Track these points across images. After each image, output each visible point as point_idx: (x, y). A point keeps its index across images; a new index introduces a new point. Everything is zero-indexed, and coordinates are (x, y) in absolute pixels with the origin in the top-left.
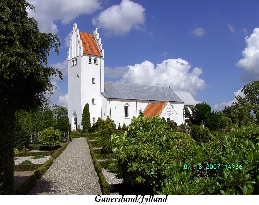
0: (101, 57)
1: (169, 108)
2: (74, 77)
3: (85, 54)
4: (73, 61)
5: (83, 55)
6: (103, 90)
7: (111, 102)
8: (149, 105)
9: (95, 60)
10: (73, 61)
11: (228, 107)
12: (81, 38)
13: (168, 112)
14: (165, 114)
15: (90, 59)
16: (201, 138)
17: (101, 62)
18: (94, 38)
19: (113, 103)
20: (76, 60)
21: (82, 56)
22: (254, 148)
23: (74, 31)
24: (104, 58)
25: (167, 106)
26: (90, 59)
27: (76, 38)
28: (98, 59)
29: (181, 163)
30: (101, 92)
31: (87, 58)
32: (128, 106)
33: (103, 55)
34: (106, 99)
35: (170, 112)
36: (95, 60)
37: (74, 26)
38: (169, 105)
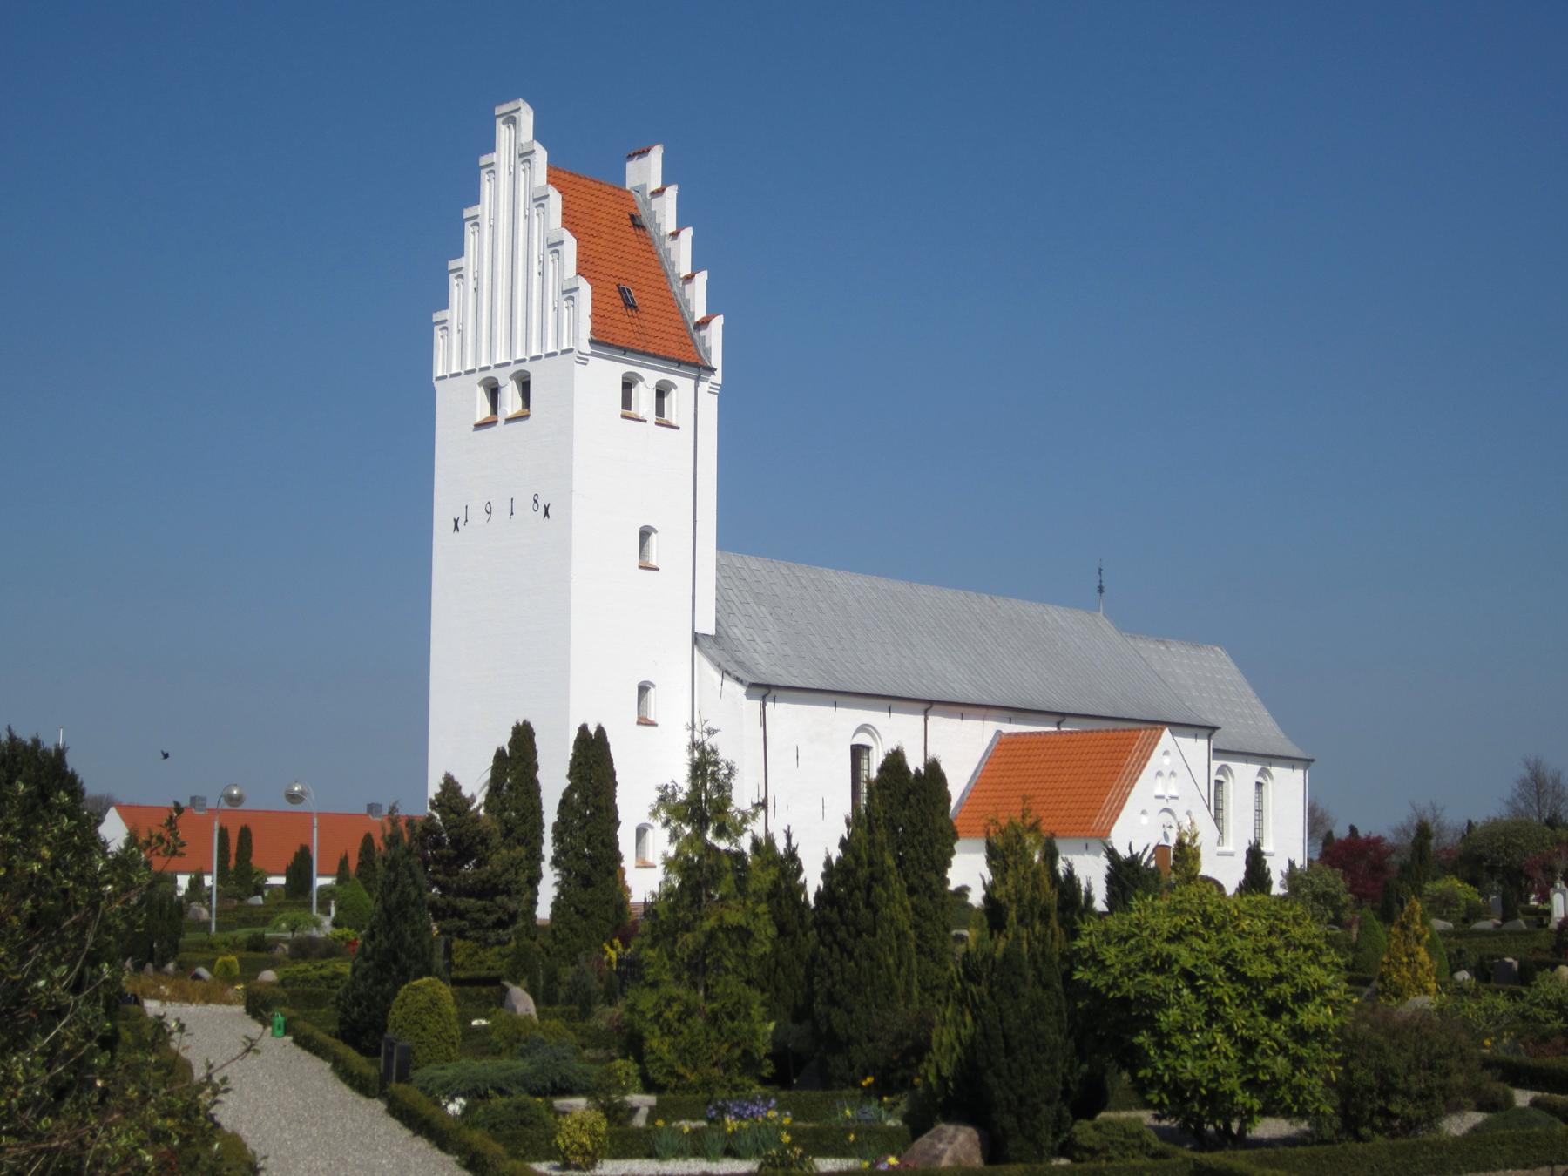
0: (701, 368)
1: (1166, 773)
2: (501, 508)
3: (604, 341)
4: (493, 392)
5: (592, 354)
6: (707, 626)
7: (770, 705)
8: (1002, 744)
9: (661, 393)
10: (493, 392)
11: (368, 840)
12: (569, 221)
13: (1163, 804)
14: (1143, 812)
15: (628, 385)
16: (967, 984)
17: (697, 403)
18: (636, 222)
19: (779, 711)
20: (525, 386)
21: (582, 360)
22: (535, 1017)
23: (503, 155)
24: (717, 378)
25: (1157, 760)
26: (628, 385)
27: (527, 217)
28: (683, 385)
29: (1288, 1142)
30: (696, 639)
31: (612, 371)
32: (868, 748)
33: (716, 360)
34: (741, 690)
35: (1171, 805)
36: (661, 393)
37: (511, 120)
38: (1166, 753)
